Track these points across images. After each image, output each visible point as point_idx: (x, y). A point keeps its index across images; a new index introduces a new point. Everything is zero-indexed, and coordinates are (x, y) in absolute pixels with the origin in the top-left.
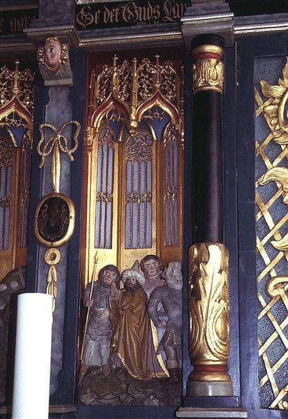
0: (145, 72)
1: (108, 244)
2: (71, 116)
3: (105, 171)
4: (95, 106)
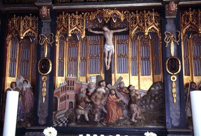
0: (149, 16)
1: (14, 76)
2: (176, 29)
3: (134, 51)
4: (183, 26)
